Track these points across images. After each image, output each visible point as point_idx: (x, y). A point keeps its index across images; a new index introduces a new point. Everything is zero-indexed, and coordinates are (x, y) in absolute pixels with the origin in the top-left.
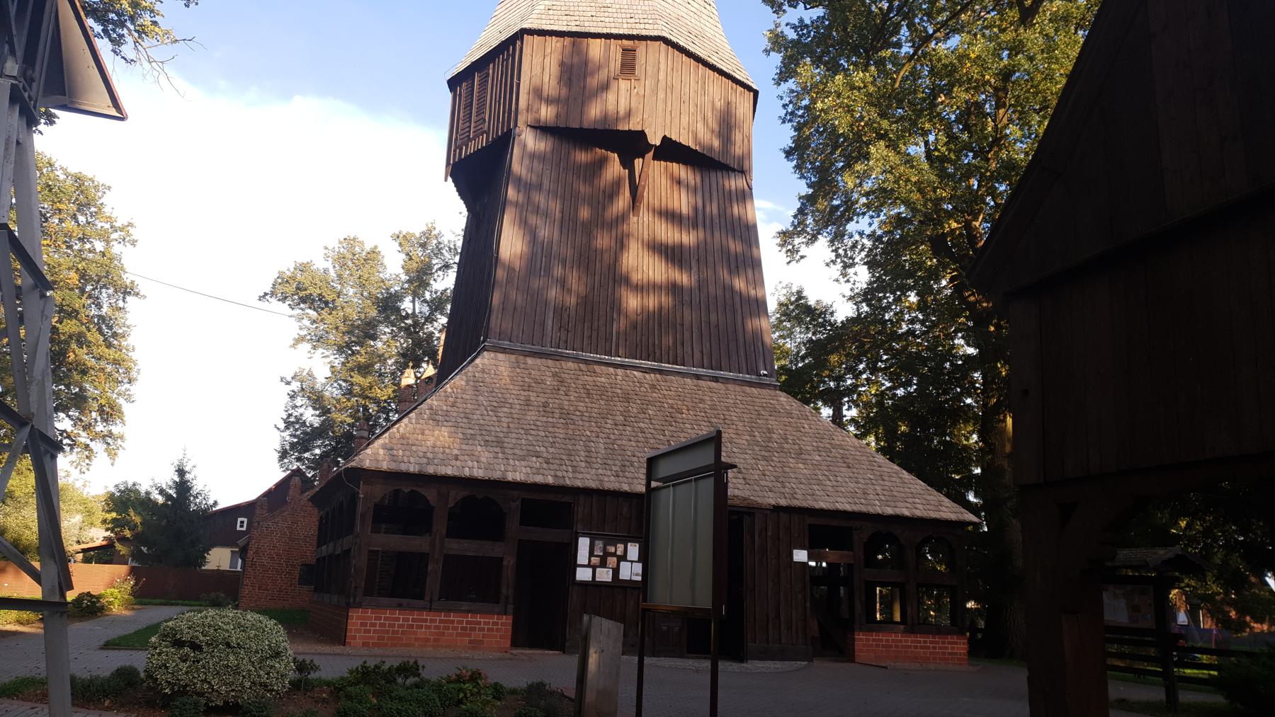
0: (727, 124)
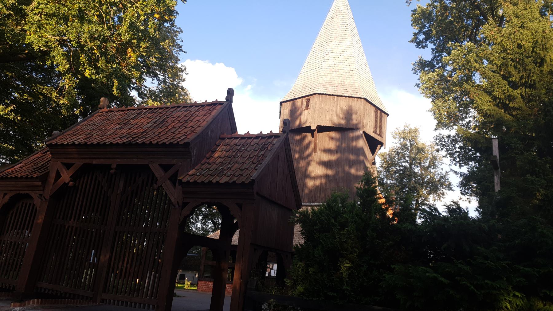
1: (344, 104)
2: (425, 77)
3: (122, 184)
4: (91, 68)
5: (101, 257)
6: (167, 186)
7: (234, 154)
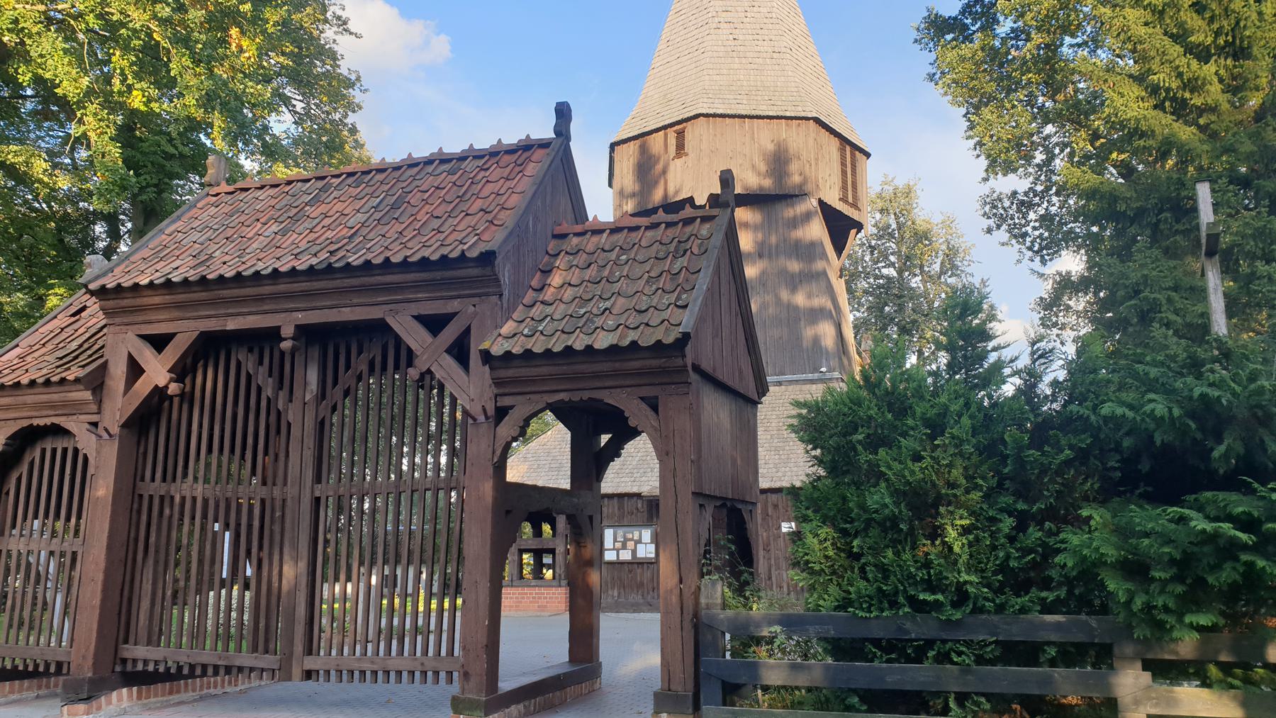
0: (779, 161)
1: (766, 136)
2: (951, 55)
3: (313, 376)
4: (145, 85)
5: (285, 568)
6: (446, 368)
7: (606, 273)
